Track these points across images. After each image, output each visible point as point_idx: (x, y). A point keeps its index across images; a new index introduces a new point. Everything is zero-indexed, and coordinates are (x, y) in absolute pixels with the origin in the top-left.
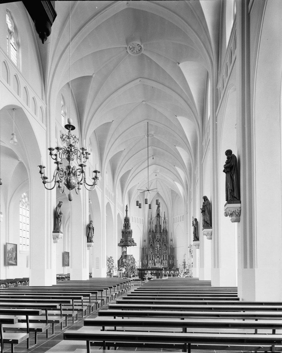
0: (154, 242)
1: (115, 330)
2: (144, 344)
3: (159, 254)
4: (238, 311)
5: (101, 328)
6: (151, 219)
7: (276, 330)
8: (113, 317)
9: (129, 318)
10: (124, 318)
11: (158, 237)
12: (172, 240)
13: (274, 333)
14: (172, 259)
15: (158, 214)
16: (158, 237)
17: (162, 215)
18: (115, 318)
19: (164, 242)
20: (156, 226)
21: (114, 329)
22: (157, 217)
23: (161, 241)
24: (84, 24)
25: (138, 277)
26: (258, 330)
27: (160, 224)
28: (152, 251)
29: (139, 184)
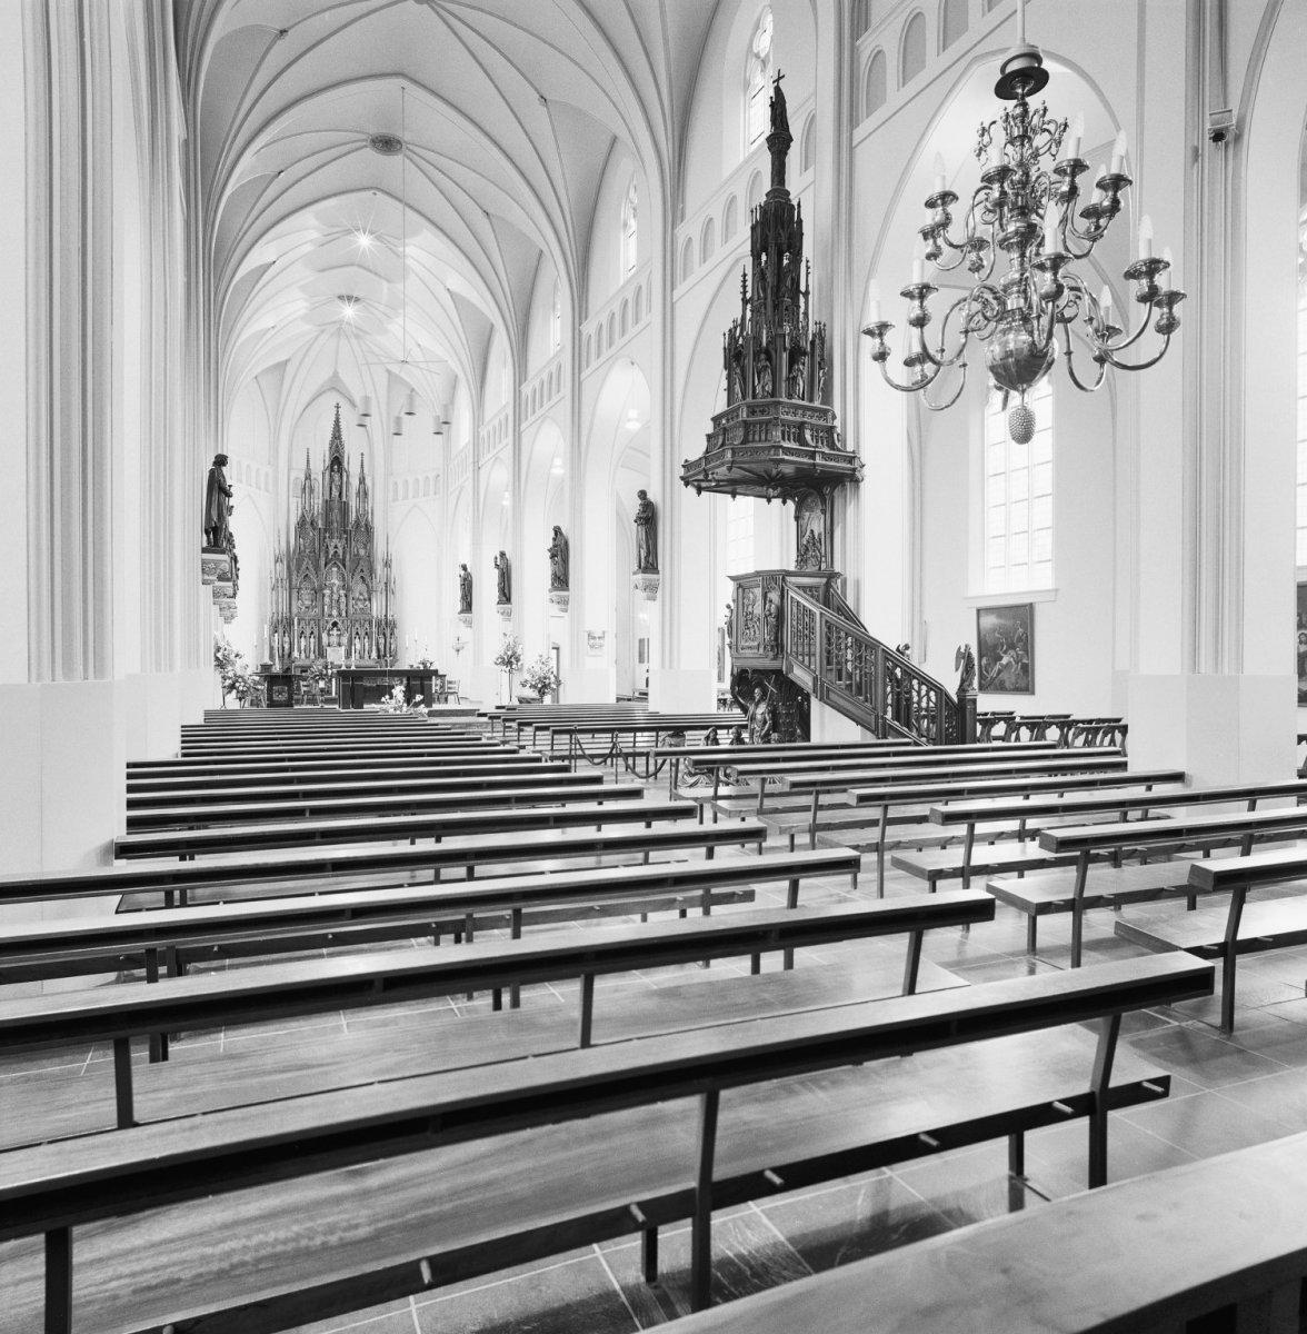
0: (317, 568)
1: (438, 880)
2: (216, 949)
3: (340, 615)
4: (206, 828)
5: (703, 850)
6: (308, 477)
7: (476, 868)
8: (643, 824)
9: (395, 845)
10: (417, 841)
11: (336, 547)
12: (387, 564)
13: (710, 855)
14: (362, 633)
15: (336, 458)
16: (336, 547)
17: (352, 466)
18: (649, 826)
19: (359, 568)
20: (328, 504)
21: (432, 879)
22: (332, 470)
23: (347, 563)
24: (1096, 86)
25: (980, 709)
26: (716, 848)
27: (344, 499)
28: (308, 603)
29: (276, 329)
